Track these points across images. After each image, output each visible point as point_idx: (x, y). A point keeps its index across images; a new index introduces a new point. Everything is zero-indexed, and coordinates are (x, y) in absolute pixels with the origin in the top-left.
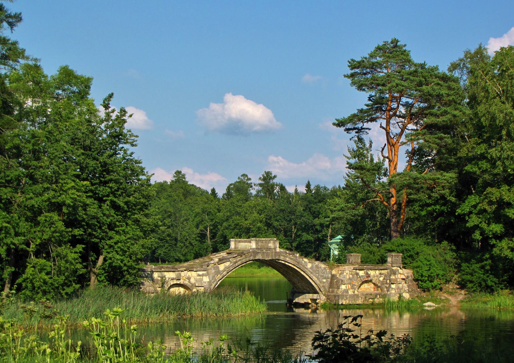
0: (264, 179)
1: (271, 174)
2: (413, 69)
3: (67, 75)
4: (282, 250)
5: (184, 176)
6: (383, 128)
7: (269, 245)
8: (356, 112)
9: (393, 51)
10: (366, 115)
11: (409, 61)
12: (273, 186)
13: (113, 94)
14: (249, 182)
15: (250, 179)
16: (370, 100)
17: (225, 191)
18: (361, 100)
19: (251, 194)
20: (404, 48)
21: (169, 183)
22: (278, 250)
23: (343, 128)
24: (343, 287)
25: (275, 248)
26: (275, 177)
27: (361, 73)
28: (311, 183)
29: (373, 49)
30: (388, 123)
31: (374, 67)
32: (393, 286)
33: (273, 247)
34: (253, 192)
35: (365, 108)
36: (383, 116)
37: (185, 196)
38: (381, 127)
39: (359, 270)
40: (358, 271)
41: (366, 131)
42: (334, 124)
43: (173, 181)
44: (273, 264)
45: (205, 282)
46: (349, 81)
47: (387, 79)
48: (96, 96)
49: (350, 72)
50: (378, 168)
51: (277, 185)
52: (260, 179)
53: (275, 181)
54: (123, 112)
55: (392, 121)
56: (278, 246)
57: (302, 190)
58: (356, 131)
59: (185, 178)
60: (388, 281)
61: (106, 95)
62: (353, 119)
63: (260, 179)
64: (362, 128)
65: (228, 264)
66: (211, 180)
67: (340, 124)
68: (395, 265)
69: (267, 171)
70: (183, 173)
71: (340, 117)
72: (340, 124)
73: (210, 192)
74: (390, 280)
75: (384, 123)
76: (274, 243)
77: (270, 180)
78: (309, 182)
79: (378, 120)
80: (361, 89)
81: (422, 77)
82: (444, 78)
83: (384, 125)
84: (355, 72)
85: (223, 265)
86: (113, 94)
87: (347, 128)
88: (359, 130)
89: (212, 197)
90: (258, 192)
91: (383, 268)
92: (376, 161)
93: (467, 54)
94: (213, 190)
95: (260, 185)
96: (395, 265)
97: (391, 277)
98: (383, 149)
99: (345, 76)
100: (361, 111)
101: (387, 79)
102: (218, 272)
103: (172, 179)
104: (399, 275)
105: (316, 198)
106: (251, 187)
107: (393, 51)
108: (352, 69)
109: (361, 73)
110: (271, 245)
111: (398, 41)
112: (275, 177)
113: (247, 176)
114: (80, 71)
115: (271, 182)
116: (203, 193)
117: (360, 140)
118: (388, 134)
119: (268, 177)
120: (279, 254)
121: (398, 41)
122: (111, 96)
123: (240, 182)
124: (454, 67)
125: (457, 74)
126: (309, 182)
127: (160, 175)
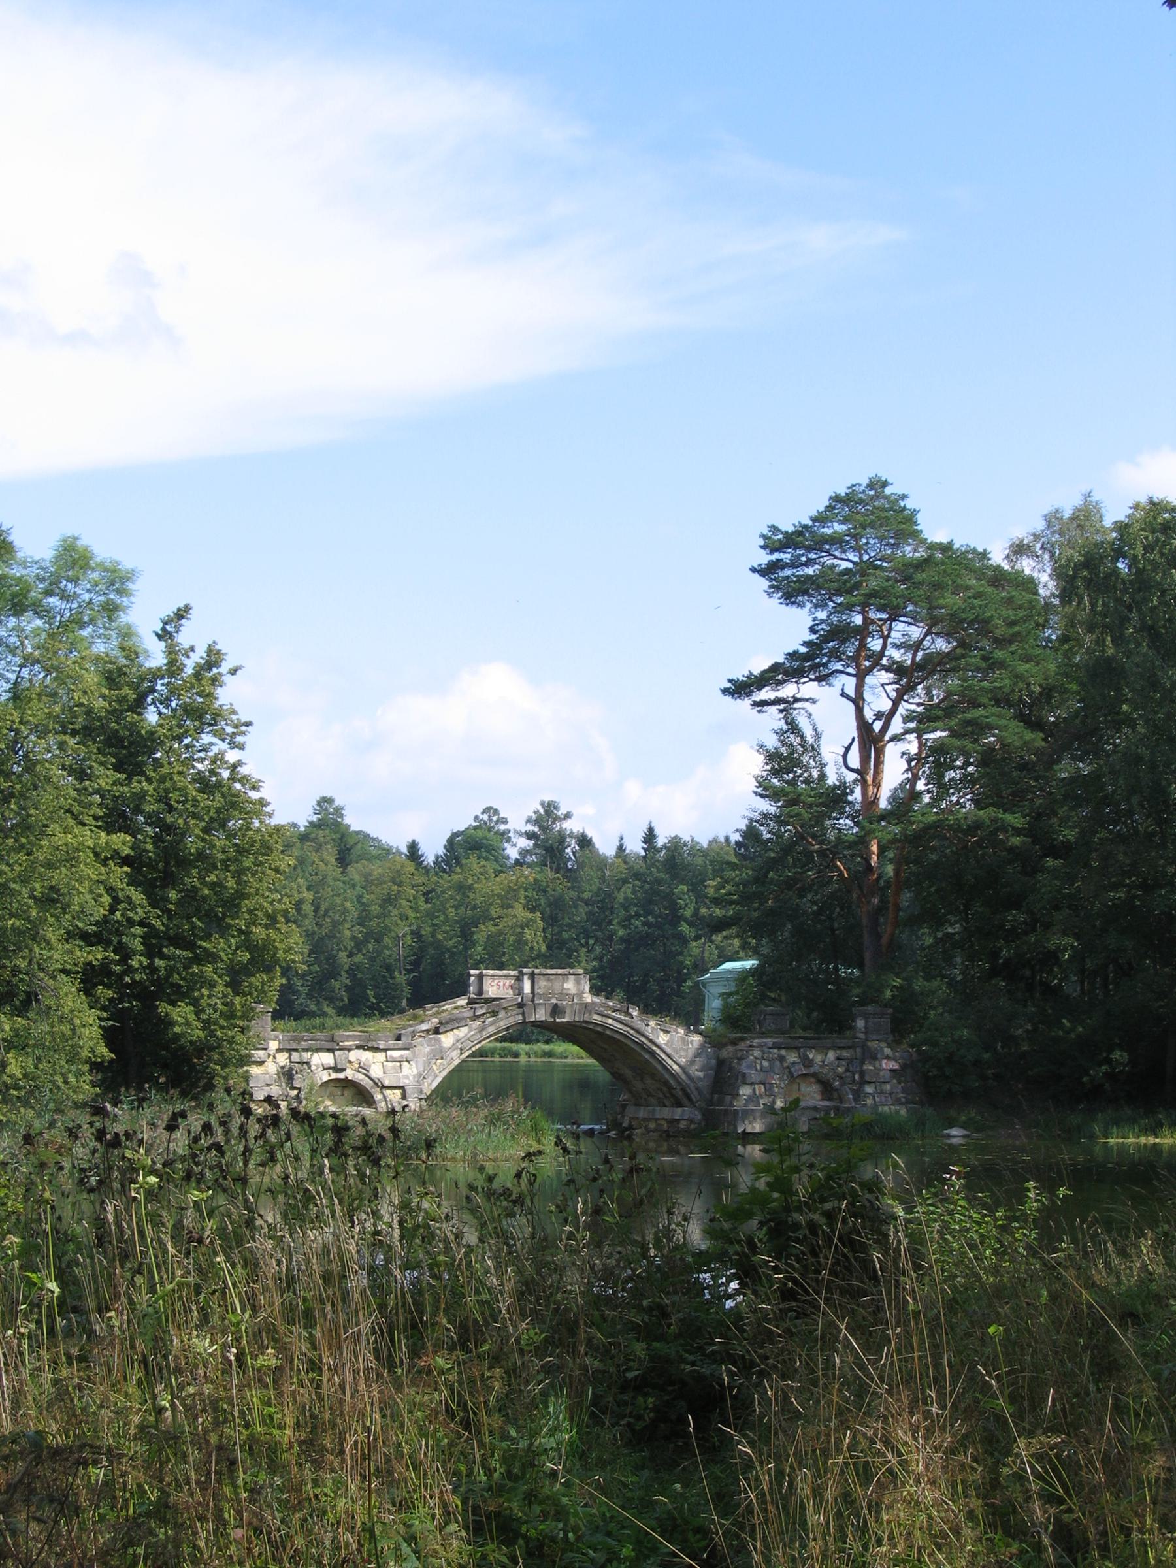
0: (538, 821)
1: (557, 808)
2: (921, 553)
3: (73, 559)
4: (596, 1000)
5: (339, 811)
6: (848, 698)
7: (566, 986)
8: (781, 659)
9: (873, 511)
10: (803, 664)
11: (915, 534)
12: (562, 838)
13: (187, 609)
14: (502, 827)
15: (504, 821)
16: (812, 630)
17: (441, 851)
18: (792, 627)
19: (508, 857)
20: (902, 504)
21: (302, 829)
22: (588, 998)
23: (747, 702)
24: (745, 1091)
25: (580, 994)
26: (568, 816)
27: (791, 563)
28: (657, 831)
29: (822, 504)
30: (859, 687)
31: (820, 543)
32: (869, 1089)
33: (573, 991)
34: (513, 853)
35: (803, 650)
36: (850, 670)
37: (343, 860)
38: (843, 695)
39: (787, 1048)
40: (783, 1052)
41: (806, 705)
42: (725, 691)
43: (311, 823)
44: (576, 1033)
45: (407, 1077)
46: (764, 583)
47: (853, 571)
48: (143, 616)
49: (764, 558)
50: (836, 798)
51: (571, 835)
52: (528, 821)
53: (568, 825)
54: (214, 658)
55: (869, 680)
56: (587, 988)
57: (635, 846)
58: (782, 707)
59: (342, 816)
60: (857, 1077)
61: (169, 610)
62: (772, 675)
63: (528, 821)
64: (796, 700)
65: (463, 1032)
66: (411, 818)
67: (739, 689)
68: (874, 1037)
69: (547, 799)
70: (337, 803)
71: (740, 674)
72: (739, 689)
73: (405, 850)
74: (862, 1073)
75: (850, 684)
76: (578, 982)
77: (554, 822)
78: (651, 830)
79: (832, 680)
80: (793, 603)
81: (944, 584)
82: (998, 578)
83: (851, 692)
84: (778, 560)
85: (450, 1034)
86: (187, 609)
87: (757, 699)
88: (786, 706)
89: (411, 867)
90: (524, 852)
91: (843, 1043)
92: (832, 780)
93: (1052, 519)
94: (413, 847)
95: (530, 836)
96: (874, 1037)
97: (865, 1067)
98: (848, 749)
99: (753, 570)
100: (793, 656)
101: (853, 571)
102: (440, 1054)
103: (310, 819)
104: (884, 1061)
105: (667, 868)
106: (509, 840)
107: (873, 511)
108: (772, 552)
109: (791, 563)
110: (570, 985)
111: (885, 484)
112: (568, 816)
113: (496, 812)
114: (103, 549)
115: (557, 827)
116: (386, 852)
117: (794, 728)
118: (859, 711)
119: (549, 814)
120: (586, 1007)
121: (885, 484)
122: (181, 614)
123: (476, 828)
124: (1019, 549)
125: (1027, 566)
126: (651, 830)
127: (287, 805)
